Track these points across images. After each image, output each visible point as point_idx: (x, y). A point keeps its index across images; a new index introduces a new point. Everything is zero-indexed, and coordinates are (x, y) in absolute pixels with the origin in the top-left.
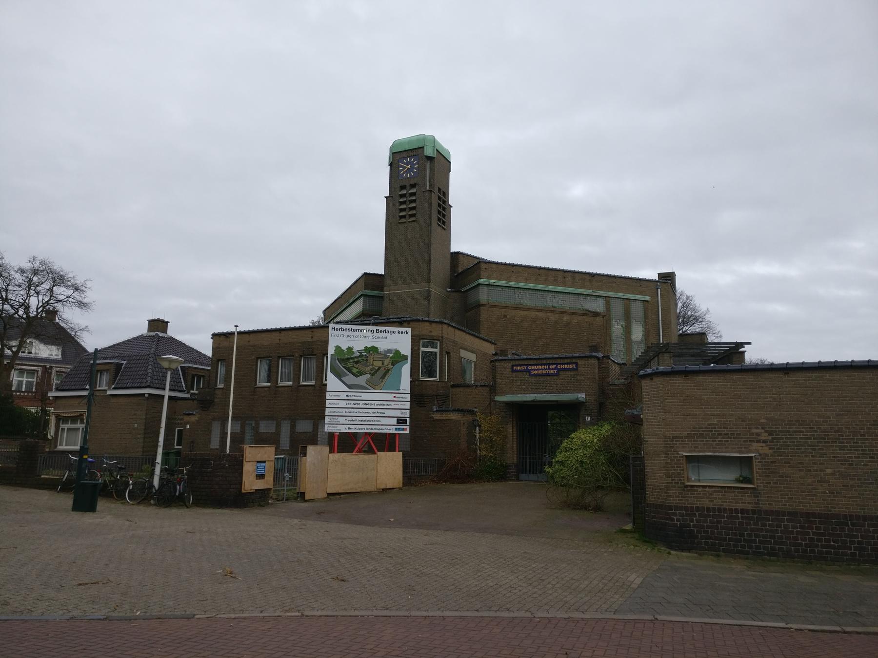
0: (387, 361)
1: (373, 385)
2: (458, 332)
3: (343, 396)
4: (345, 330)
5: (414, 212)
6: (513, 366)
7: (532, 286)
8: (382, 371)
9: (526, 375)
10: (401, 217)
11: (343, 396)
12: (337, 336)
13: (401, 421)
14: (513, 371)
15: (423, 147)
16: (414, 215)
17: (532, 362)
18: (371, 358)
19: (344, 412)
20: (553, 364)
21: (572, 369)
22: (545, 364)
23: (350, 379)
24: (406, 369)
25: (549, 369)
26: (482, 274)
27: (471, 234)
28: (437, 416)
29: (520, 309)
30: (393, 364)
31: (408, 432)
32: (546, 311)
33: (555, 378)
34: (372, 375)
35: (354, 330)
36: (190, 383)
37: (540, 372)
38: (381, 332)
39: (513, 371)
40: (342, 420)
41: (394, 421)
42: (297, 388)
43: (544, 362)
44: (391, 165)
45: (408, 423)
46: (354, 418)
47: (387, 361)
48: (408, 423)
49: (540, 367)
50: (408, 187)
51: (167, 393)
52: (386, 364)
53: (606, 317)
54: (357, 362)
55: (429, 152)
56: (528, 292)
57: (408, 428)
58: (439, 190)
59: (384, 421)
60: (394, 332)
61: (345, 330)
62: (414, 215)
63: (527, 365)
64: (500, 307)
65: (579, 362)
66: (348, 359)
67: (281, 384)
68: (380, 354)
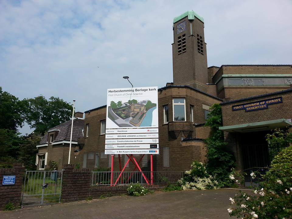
0: (143, 108)
1: (134, 124)
3: (116, 131)
4: (117, 91)
7: (254, 75)
8: (140, 115)
9: (243, 112)
11: (116, 131)
12: (112, 95)
13: (153, 146)
14: (233, 110)
15: (187, 16)
16: (185, 49)
18: (133, 107)
19: (116, 141)
20: (262, 101)
22: (256, 102)
23: (120, 121)
24: (155, 113)
26: (224, 72)
27: (218, 53)
29: (249, 88)
30: (147, 110)
31: (158, 153)
32: (265, 88)
33: (265, 110)
34: (133, 117)
35: (122, 91)
37: (253, 108)
38: (138, 90)
39: (233, 110)
40: (115, 147)
41: (148, 146)
44: (173, 30)
45: (158, 147)
46: (129, 145)
47: (143, 108)
48: (158, 147)
49: (253, 105)
51: (71, 142)
52: (142, 110)
54: (124, 110)
55: (191, 17)
56: (252, 79)
57: (158, 150)
58: (198, 35)
59: (142, 146)
60: (147, 90)
61: (117, 91)
63: (243, 105)
64: (236, 88)
66: (119, 109)
68: (139, 104)
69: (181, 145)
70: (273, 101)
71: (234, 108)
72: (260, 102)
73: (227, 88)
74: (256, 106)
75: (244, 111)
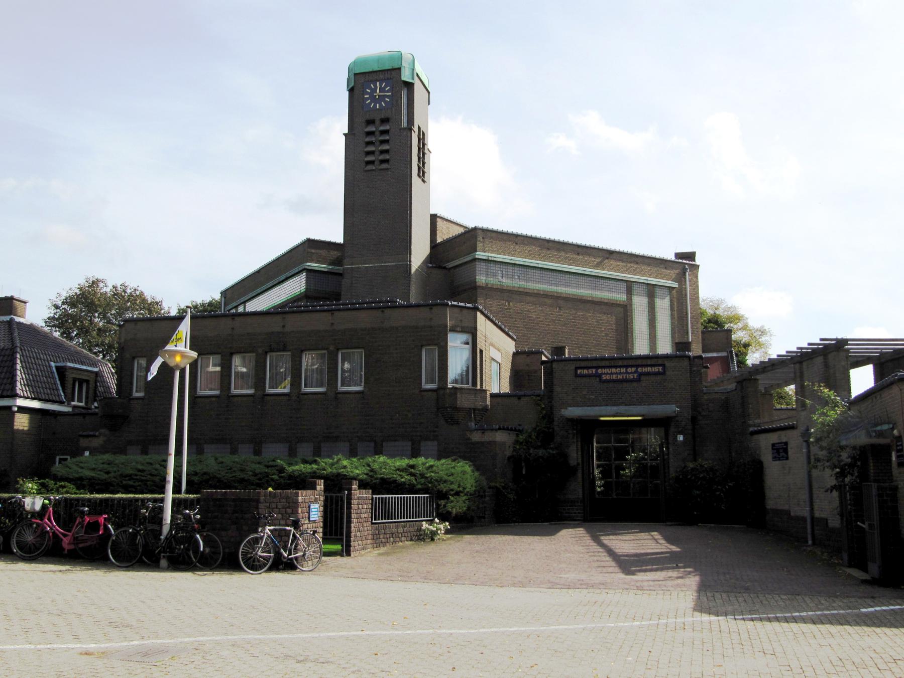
2: (668, 312)
5: (387, 157)
6: (577, 368)
10: (368, 163)
14: (576, 375)
15: (400, 69)
16: (387, 161)
17: (603, 363)
20: (632, 366)
21: (658, 373)
22: (620, 367)
25: (627, 373)
26: (480, 245)
27: (466, 180)
28: (476, 437)
33: (635, 384)
36: (69, 391)
37: (614, 377)
42: (261, 398)
43: (620, 363)
44: (351, 91)
49: (614, 370)
50: (378, 122)
53: (625, 312)
55: (406, 76)
62: (387, 161)
63: (597, 368)
65: (668, 364)
67: (235, 391)
69: (469, 439)
70: (649, 369)
71: (579, 372)
72: (627, 367)
73: (482, 287)
74: (620, 373)
75: (598, 379)
